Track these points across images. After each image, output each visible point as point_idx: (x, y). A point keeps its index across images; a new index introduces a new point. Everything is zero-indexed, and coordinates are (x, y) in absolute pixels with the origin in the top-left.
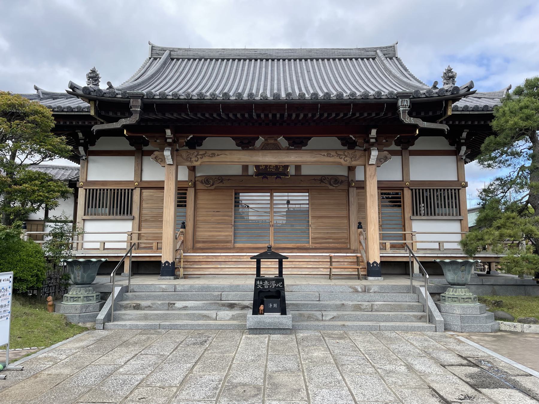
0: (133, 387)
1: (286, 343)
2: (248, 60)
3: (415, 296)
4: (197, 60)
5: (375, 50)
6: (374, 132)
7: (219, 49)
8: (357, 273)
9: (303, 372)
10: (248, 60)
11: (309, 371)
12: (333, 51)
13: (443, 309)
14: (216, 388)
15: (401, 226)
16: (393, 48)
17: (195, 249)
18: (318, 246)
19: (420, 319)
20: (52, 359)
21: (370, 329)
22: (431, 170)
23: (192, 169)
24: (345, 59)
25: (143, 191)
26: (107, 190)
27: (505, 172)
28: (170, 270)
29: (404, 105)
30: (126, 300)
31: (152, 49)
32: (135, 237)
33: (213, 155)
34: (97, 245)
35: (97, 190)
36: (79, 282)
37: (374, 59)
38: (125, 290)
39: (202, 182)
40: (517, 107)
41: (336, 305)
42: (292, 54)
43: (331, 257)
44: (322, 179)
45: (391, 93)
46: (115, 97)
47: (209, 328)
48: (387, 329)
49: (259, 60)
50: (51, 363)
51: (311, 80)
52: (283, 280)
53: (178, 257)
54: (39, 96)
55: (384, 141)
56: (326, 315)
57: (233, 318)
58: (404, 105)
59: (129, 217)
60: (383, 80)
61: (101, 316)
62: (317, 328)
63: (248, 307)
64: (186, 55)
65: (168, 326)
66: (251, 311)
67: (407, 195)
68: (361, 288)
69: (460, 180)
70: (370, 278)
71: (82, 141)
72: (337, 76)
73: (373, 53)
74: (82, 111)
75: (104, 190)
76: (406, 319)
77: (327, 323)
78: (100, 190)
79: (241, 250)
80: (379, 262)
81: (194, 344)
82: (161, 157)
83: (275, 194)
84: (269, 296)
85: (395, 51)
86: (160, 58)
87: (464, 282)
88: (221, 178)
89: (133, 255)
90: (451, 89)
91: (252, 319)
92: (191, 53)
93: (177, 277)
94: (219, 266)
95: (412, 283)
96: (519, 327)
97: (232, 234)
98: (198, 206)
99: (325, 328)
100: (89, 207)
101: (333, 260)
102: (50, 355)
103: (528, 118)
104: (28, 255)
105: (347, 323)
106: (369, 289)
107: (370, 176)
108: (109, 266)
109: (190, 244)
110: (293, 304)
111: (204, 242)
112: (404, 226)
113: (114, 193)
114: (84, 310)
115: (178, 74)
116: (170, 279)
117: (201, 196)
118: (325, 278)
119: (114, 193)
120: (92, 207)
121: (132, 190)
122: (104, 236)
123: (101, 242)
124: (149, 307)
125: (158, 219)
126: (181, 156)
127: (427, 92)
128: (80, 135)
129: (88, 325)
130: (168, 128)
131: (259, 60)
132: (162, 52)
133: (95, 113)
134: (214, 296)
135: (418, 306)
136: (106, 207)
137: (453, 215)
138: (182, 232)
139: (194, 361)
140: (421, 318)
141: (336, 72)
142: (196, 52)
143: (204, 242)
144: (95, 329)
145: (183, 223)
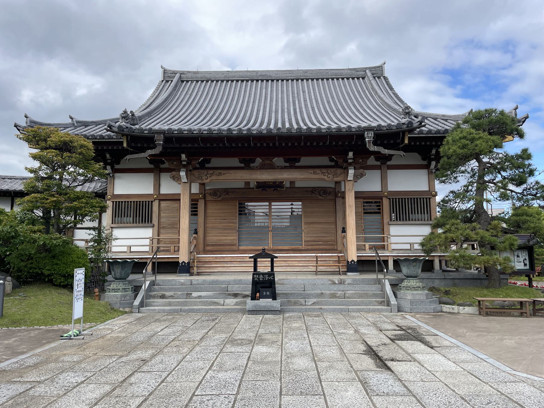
0: (170, 341)
1: (275, 319)
2: (250, 81)
3: (379, 286)
4: (205, 82)
5: (364, 70)
6: (351, 154)
7: (224, 72)
8: (338, 270)
9: (283, 333)
10: (250, 81)
11: (287, 333)
12: (327, 71)
13: (399, 296)
14: (224, 341)
15: (381, 230)
16: (380, 68)
17: (205, 252)
18: (310, 247)
19: (381, 303)
20: (109, 329)
21: (341, 311)
22: (408, 182)
23: (202, 185)
24: (338, 79)
25: (161, 202)
26: (131, 202)
27: (456, 187)
28: (186, 269)
29: (369, 137)
30: (154, 291)
31: (164, 73)
32: (155, 241)
33: (220, 174)
34: (125, 249)
35: (122, 202)
36: (118, 277)
37: (363, 78)
38: (153, 283)
39: (210, 194)
40: (458, 138)
41: (317, 294)
42: (290, 75)
43: (317, 257)
44: (313, 190)
45: (359, 127)
46: (143, 133)
47: (218, 311)
49: (260, 81)
50: (110, 331)
51: (305, 101)
52: (274, 275)
53: (192, 258)
54: (74, 124)
55: (361, 160)
56: (308, 301)
57: (237, 304)
58: (369, 137)
59: (150, 224)
60: (369, 100)
61: (137, 302)
62: (300, 311)
63: (248, 296)
64: (194, 77)
65: (187, 310)
66: (250, 298)
67: (386, 203)
68: (338, 281)
69: (431, 190)
70: (349, 274)
71: (109, 161)
72: (329, 96)
73: (363, 73)
74: (112, 138)
75: (128, 202)
76: (370, 304)
77: (308, 307)
78: (125, 202)
79: (245, 252)
80: (356, 260)
81: (208, 320)
82: (177, 176)
83: (273, 203)
84: (264, 286)
85: (382, 71)
86: (172, 81)
87: (415, 275)
88: (227, 191)
89: (158, 256)
90: (407, 123)
91: (250, 304)
92: (199, 76)
93: (192, 274)
94: (226, 265)
95: (377, 276)
96: (456, 308)
97: (237, 238)
99: (306, 310)
100: (115, 217)
101: (341, 259)
102: (107, 327)
103: (464, 147)
104: (78, 258)
105: (323, 307)
106: (344, 282)
107: (349, 190)
108: (138, 266)
109: (201, 247)
110: (283, 293)
111: (213, 245)
112: (383, 230)
113: (137, 204)
114: (123, 299)
115: (188, 96)
116: (186, 276)
118: (313, 274)
119: (137, 204)
120: (119, 217)
121: (152, 202)
122: (131, 241)
123: (127, 246)
124: (172, 297)
125: (175, 226)
126: (194, 175)
127: (388, 126)
128: (108, 156)
129: (127, 310)
130: (183, 153)
131: (260, 81)
132: (173, 75)
133: (128, 145)
134: (222, 288)
135: (381, 294)
136: (130, 216)
137: (424, 220)
138: (195, 237)
139: (208, 329)
140: (381, 303)
141: (328, 92)
142: (204, 75)
143: (213, 245)
144: (132, 312)
145: (196, 230)
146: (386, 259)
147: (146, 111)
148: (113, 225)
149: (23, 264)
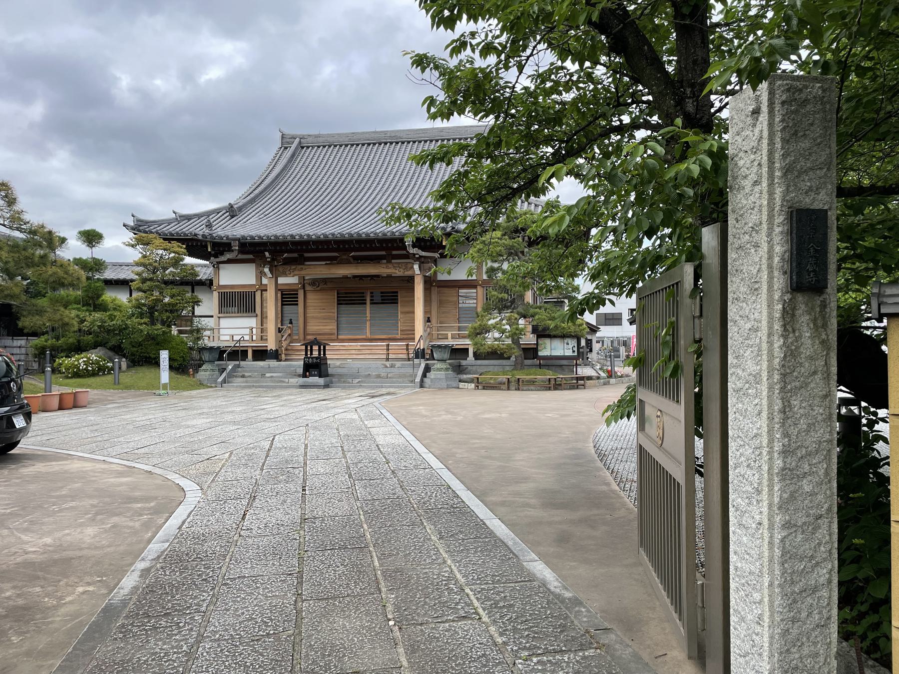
28: (275, 355)
29: (408, 241)
31: (282, 138)
34: (228, 338)
48: (829, 466)
59: (254, 314)
61: (220, 380)
74: (81, 549)
91: (302, 380)
92: (320, 140)
97: (335, 327)
98: (308, 304)
117: (310, 296)
122: (234, 330)
146: (466, 347)
147: (249, 198)
148: (220, 315)
149: (135, 349)
